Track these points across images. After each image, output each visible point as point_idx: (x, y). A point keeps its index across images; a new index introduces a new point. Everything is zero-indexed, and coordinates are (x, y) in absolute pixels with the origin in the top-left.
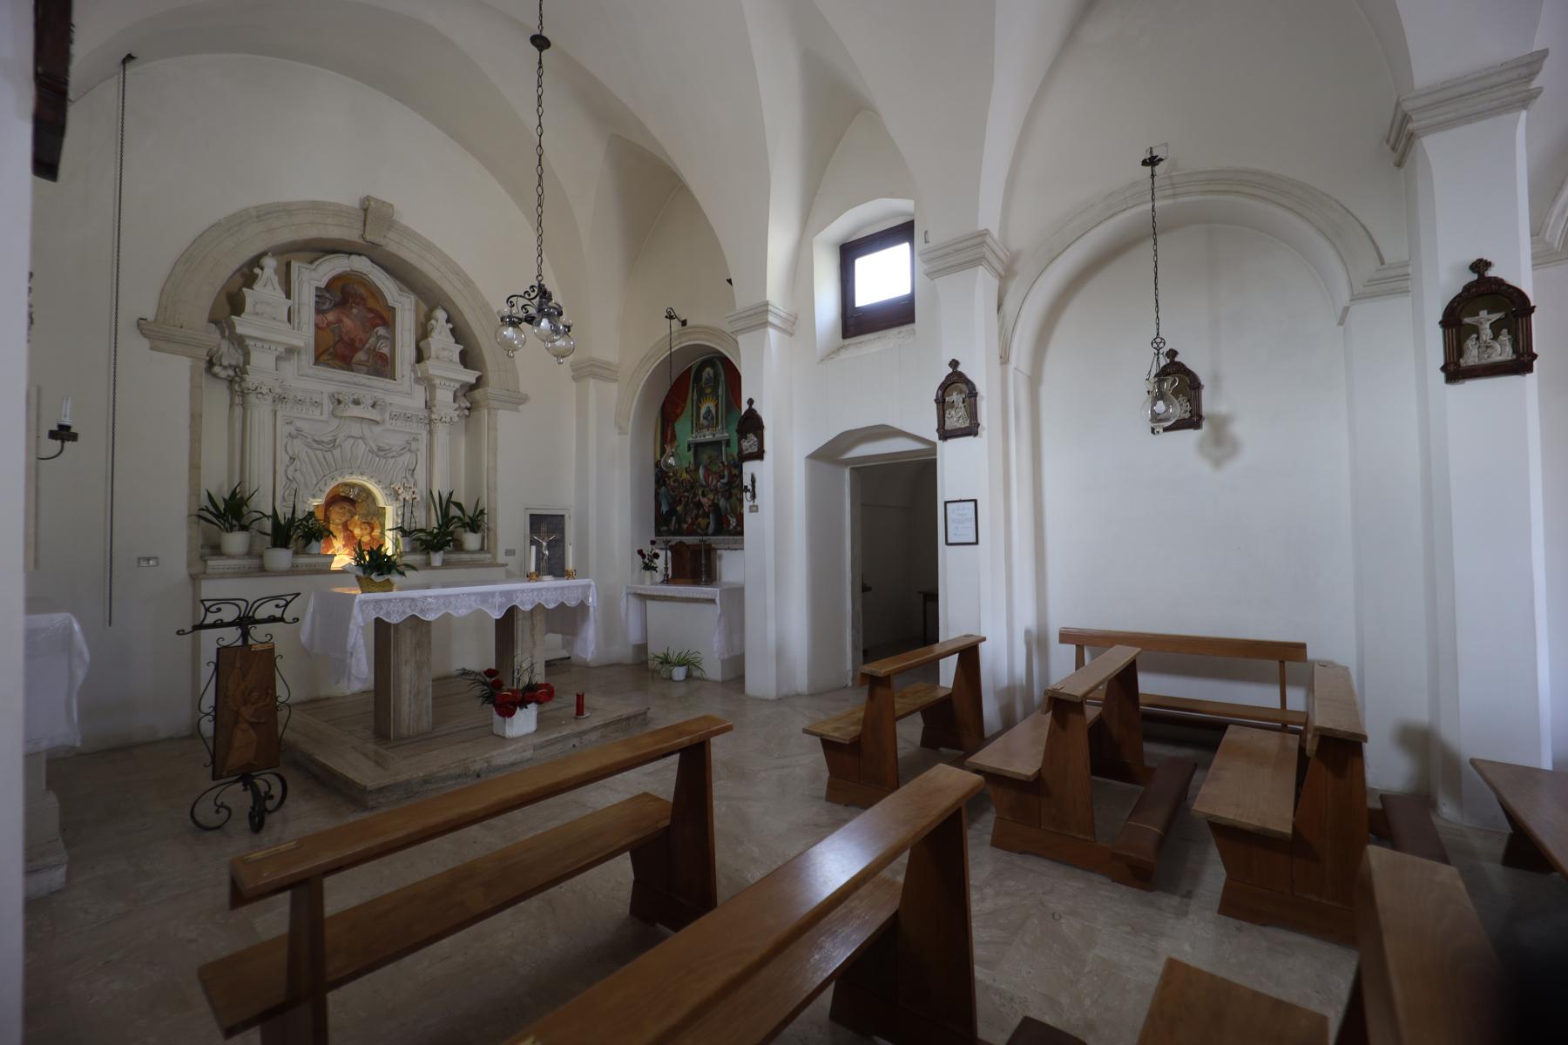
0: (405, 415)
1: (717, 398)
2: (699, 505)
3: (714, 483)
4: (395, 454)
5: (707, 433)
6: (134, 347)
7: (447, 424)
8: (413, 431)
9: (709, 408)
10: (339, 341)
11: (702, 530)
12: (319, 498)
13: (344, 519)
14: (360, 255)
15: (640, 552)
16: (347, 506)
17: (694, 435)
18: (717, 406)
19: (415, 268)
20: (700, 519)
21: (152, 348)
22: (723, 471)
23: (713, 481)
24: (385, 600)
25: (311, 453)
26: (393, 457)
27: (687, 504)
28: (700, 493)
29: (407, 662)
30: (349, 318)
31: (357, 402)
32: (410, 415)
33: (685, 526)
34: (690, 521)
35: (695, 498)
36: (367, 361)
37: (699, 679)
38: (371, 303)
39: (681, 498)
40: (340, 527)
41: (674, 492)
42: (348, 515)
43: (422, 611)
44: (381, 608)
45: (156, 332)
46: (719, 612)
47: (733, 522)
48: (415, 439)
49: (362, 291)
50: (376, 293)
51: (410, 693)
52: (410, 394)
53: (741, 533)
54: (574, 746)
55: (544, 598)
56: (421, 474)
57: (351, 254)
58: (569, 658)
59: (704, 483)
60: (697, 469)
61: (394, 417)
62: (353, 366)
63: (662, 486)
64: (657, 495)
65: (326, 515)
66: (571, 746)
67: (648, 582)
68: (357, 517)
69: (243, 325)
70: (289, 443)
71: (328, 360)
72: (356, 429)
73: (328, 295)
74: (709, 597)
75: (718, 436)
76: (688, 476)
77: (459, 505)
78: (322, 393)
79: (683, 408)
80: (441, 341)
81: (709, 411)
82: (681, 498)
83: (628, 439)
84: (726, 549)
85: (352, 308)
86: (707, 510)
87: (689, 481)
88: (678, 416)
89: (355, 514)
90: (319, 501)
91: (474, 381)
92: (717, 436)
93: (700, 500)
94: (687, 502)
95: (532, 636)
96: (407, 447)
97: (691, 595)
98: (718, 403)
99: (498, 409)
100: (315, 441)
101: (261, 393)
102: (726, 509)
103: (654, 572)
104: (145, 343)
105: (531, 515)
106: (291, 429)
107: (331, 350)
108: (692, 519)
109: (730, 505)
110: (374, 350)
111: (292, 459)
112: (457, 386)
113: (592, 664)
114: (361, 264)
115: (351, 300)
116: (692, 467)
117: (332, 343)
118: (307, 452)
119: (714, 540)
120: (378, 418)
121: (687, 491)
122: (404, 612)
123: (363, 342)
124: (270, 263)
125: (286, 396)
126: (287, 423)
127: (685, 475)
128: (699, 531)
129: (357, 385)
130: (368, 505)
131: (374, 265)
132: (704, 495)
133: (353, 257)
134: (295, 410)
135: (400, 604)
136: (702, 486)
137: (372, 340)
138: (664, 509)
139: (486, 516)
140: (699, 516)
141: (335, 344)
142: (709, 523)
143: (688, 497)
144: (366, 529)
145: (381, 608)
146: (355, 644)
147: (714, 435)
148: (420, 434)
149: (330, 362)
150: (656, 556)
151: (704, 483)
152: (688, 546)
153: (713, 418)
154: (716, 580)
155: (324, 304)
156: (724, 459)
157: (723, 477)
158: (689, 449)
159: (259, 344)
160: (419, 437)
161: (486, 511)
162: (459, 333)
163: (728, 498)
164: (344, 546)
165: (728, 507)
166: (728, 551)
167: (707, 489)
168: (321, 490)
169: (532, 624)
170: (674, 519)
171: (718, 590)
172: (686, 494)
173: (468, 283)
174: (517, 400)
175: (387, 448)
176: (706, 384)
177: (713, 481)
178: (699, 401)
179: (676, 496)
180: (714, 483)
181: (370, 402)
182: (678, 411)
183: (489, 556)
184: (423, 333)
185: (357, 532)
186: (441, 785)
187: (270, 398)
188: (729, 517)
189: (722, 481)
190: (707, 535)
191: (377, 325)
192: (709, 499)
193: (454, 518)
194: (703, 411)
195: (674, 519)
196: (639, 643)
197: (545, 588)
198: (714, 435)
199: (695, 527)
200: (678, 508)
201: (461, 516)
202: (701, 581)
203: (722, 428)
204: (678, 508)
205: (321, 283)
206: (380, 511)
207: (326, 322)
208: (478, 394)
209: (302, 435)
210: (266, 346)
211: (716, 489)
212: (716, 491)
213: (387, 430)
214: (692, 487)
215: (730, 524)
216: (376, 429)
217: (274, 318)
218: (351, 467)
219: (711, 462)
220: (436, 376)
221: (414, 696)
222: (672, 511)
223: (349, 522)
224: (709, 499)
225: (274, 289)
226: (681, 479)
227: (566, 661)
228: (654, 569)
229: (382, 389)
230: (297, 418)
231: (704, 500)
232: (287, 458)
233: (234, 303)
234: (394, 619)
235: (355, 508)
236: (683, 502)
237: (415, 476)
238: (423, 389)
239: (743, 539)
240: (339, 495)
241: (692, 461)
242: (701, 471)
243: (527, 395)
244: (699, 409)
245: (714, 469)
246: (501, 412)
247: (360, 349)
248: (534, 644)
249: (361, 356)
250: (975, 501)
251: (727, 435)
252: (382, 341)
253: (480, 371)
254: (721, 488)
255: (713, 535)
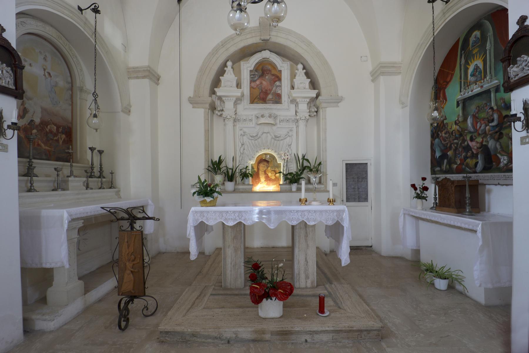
0: (286, 119)
1: (486, 53)
2: (468, 148)
3: (482, 128)
4: (282, 138)
5: (475, 87)
6: (187, 107)
7: (304, 121)
8: (290, 126)
9: (477, 64)
10: (261, 92)
11: (470, 168)
12: (252, 160)
13: (264, 169)
14: (265, 50)
15: (413, 186)
16: (266, 163)
17: (462, 93)
18: (485, 62)
19: (285, 46)
20: (468, 160)
21: (193, 108)
22: (492, 115)
23: (481, 127)
24: (206, 211)
25: (250, 141)
26: (282, 140)
27: (456, 149)
28: (468, 138)
29: (229, 246)
30: (265, 81)
31: (263, 116)
32: (288, 119)
33: (455, 166)
34: (459, 162)
35: (464, 143)
36: (273, 98)
37: (461, 293)
38: (273, 72)
39: (451, 145)
40: (263, 173)
41: (445, 141)
42: (266, 167)
43: (226, 219)
44: (204, 216)
45: (194, 102)
46: (480, 243)
47: (504, 160)
48: (291, 130)
49: (270, 67)
50: (274, 67)
51: (231, 263)
52: (288, 109)
53: (510, 170)
54: (306, 341)
55: (305, 217)
56: (294, 146)
57: (261, 51)
58: (371, 247)
59: (472, 130)
60: (465, 120)
61: (282, 121)
62: (267, 101)
63: (436, 139)
64: (432, 145)
65: (258, 167)
66: (303, 340)
67: (419, 207)
68: (269, 168)
69: (219, 92)
70: (241, 138)
71: (257, 101)
72: (266, 129)
73: (256, 73)
74: (471, 227)
75: (486, 86)
76: (458, 127)
77: (307, 160)
78: (252, 115)
79: (453, 75)
80: (301, 80)
81: (477, 68)
82: (451, 145)
83: (407, 109)
84: (496, 185)
85: (266, 76)
86: (475, 152)
87: (458, 130)
88: (448, 83)
89: (269, 167)
90: (252, 162)
91: (315, 96)
92: (484, 86)
93: (468, 144)
94: (456, 149)
95: (306, 240)
96: (287, 135)
97: (452, 223)
98: (486, 58)
99: (326, 107)
100: (251, 137)
101: (228, 118)
102: (496, 148)
103: (424, 201)
104: (191, 106)
105: (346, 164)
106: (242, 132)
107: (258, 97)
108: (460, 160)
109: (500, 145)
110: (275, 93)
111: (242, 145)
112: (308, 100)
113: (383, 254)
114: (266, 54)
115: (265, 73)
116: (461, 119)
117: (258, 94)
118: (248, 141)
119: (482, 177)
120: (272, 122)
121: (456, 138)
122: (235, 220)
123: (271, 90)
124: (229, 64)
125: (239, 119)
126: (240, 130)
127: (455, 127)
128: (468, 169)
129: (266, 109)
130: (274, 163)
131: (272, 53)
132: (472, 140)
133: (262, 52)
134: (249, 124)
135: (214, 214)
136: (470, 132)
137: (274, 89)
138: (438, 154)
139: (322, 165)
140: (468, 158)
141: (260, 93)
142: (478, 162)
143: (457, 144)
144: (273, 173)
145: (204, 216)
146: (189, 234)
147: (482, 87)
148: (293, 128)
149: (258, 102)
150: (426, 189)
151: (472, 130)
152: (453, 182)
153: (481, 72)
154: (484, 210)
155: (255, 77)
156: (493, 104)
157: (493, 121)
158: (458, 105)
159: (227, 99)
160: (293, 129)
161: (322, 163)
162: (308, 74)
163: (498, 140)
164: (265, 181)
165: (498, 146)
166: (499, 186)
167: (476, 134)
168: (252, 157)
169: (306, 233)
170: (445, 161)
171: (481, 222)
172: (456, 141)
173: (309, 44)
174: (337, 101)
175: (279, 136)
176: (473, 46)
177: (481, 127)
178: (467, 63)
179: (447, 144)
180: (482, 128)
181: (268, 115)
182: (448, 79)
183: (323, 186)
184: (293, 76)
185: (270, 174)
186: (203, 340)
187: (232, 120)
188: (499, 156)
189: (490, 124)
190: (475, 172)
191: (276, 81)
192: (477, 142)
193: (306, 167)
194: (470, 71)
195: (445, 161)
196: (415, 248)
197: (307, 211)
198: (482, 87)
199: (464, 166)
200: (448, 153)
201: (309, 165)
202: (465, 211)
203: (491, 78)
204: (448, 153)
205: (252, 68)
206: (279, 165)
207: (256, 85)
208: (318, 102)
209: (246, 134)
210: (229, 99)
211: (485, 133)
212: (485, 134)
213: (278, 127)
214: (461, 135)
215: (500, 162)
216: (274, 128)
217: (231, 87)
218: (264, 146)
219: (479, 111)
220: (298, 97)
221: (233, 266)
222: (444, 156)
223: (266, 170)
224: (477, 142)
225: (231, 74)
226: (451, 130)
227: (369, 248)
228: (425, 198)
229: (276, 109)
230: (243, 127)
231: (472, 144)
232: (240, 145)
233: (216, 83)
234: (211, 223)
235: (268, 164)
236: (453, 147)
237: (291, 148)
238: (295, 105)
239: (512, 176)
240: (262, 159)
241: (461, 114)
242: (469, 121)
243: (342, 97)
244: (466, 69)
245: (483, 115)
246: (328, 109)
247: (269, 94)
248: (308, 246)
249: (270, 97)
250: (367, 61)
251: (497, 81)
252: (278, 88)
253: (317, 89)
254: (489, 131)
255: (481, 172)
